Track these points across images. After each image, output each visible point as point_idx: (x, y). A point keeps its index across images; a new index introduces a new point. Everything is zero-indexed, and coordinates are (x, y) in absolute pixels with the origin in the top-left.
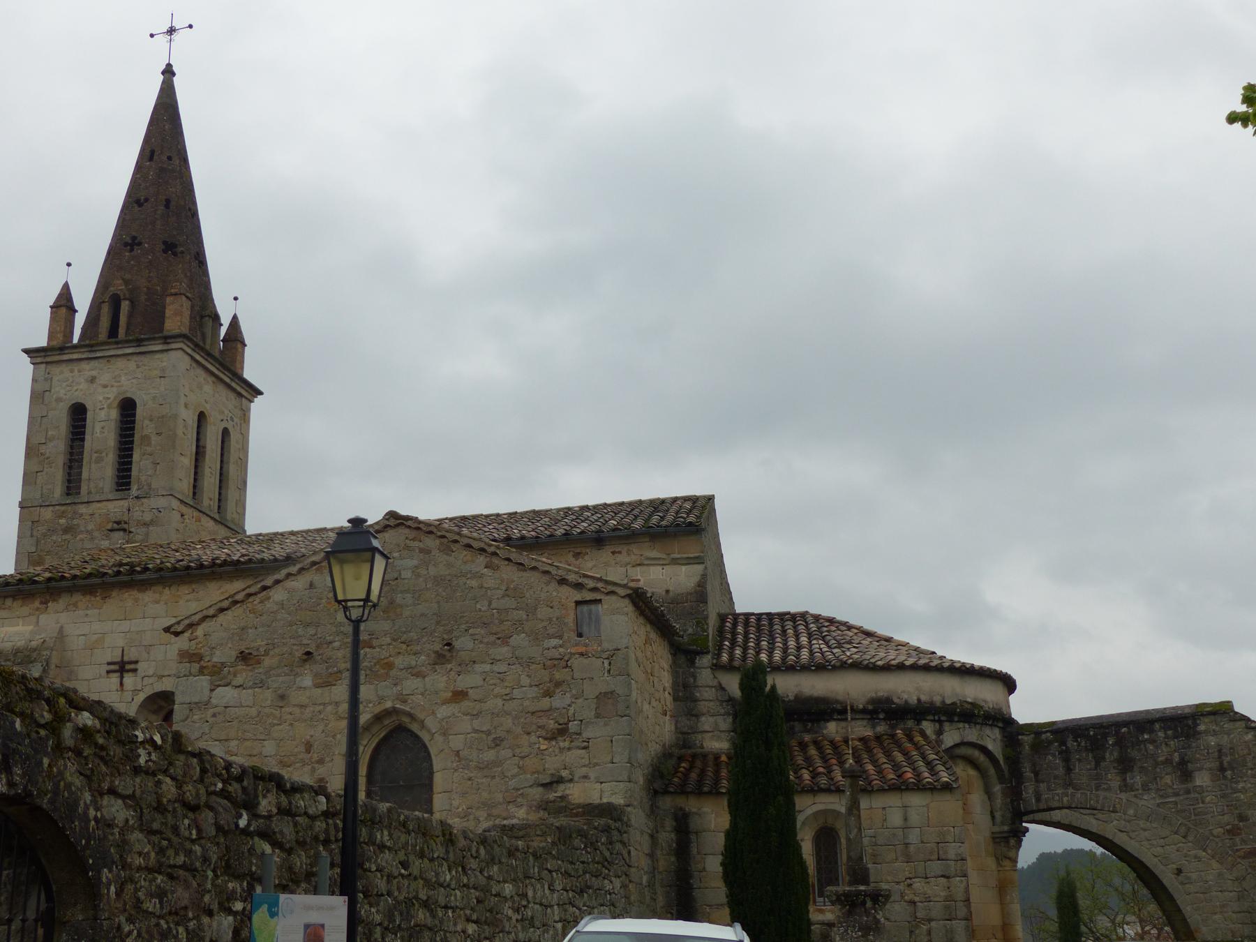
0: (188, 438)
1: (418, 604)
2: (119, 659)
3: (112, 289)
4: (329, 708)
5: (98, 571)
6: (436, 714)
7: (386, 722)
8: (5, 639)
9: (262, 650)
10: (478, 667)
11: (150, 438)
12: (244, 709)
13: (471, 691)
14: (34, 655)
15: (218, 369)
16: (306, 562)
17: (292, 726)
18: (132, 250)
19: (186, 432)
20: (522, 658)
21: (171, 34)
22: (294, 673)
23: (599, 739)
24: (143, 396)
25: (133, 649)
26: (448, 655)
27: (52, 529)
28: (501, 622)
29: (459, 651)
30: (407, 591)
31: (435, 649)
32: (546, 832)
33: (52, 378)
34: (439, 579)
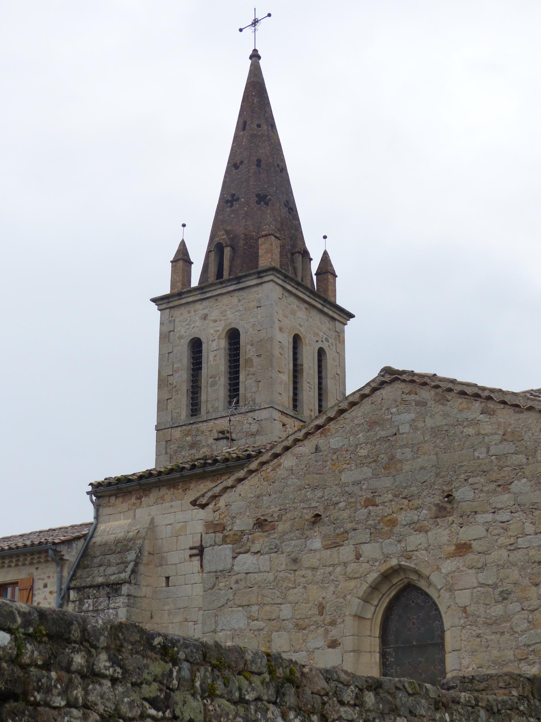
0: (285, 358)
1: (418, 457)
2: (198, 544)
4: (339, 569)
5: (178, 466)
6: (441, 569)
7: (395, 581)
9: (275, 515)
10: (480, 518)
11: (252, 360)
12: (262, 574)
13: (474, 544)
15: (309, 296)
16: (310, 427)
17: (305, 589)
18: (231, 206)
19: (282, 352)
21: (255, 25)
22: (305, 536)
24: (245, 325)
26: (448, 506)
28: (501, 468)
30: (406, 446)
31: (436, 502)
32: (509, 684)
33: (175, 319)
34: (436, 430)
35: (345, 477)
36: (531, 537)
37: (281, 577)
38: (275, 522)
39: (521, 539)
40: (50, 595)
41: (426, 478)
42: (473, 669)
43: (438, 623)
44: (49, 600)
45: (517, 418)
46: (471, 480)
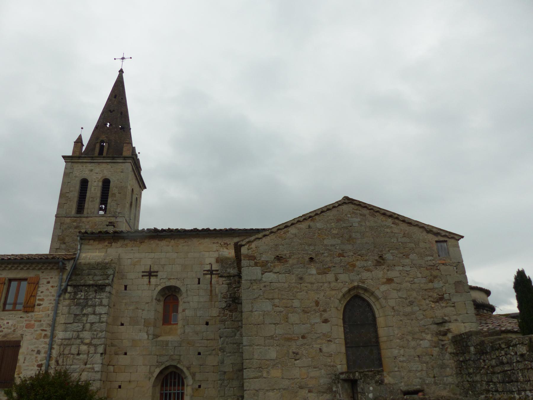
2: (148, 270)
3: (101, 138)
4: (326, 285)
6: (380, 289)
8: (91, 258)
9: (288, 255)
10: (397, 268)
12: (281, 284)
13: (395, 279)
14: (108, 265)
17: (307, 293)
20: (416, 265)
23: (459, 303)
25: (155, 266)
27: (70, 227)
28: (404, 248)
29: (387, 260)
30: (357, 232)
31: (376, 259)
35: (325, 242)
36: (420, 278)
37: (293, 286)
38: (287, 259)
39: (416, 279)
40: (52, 288)
41: (369, 248)
42: (400, 335)
43: (370, 314)
44: (50, 291)
45: (409, 228)
46: (390, 251)
